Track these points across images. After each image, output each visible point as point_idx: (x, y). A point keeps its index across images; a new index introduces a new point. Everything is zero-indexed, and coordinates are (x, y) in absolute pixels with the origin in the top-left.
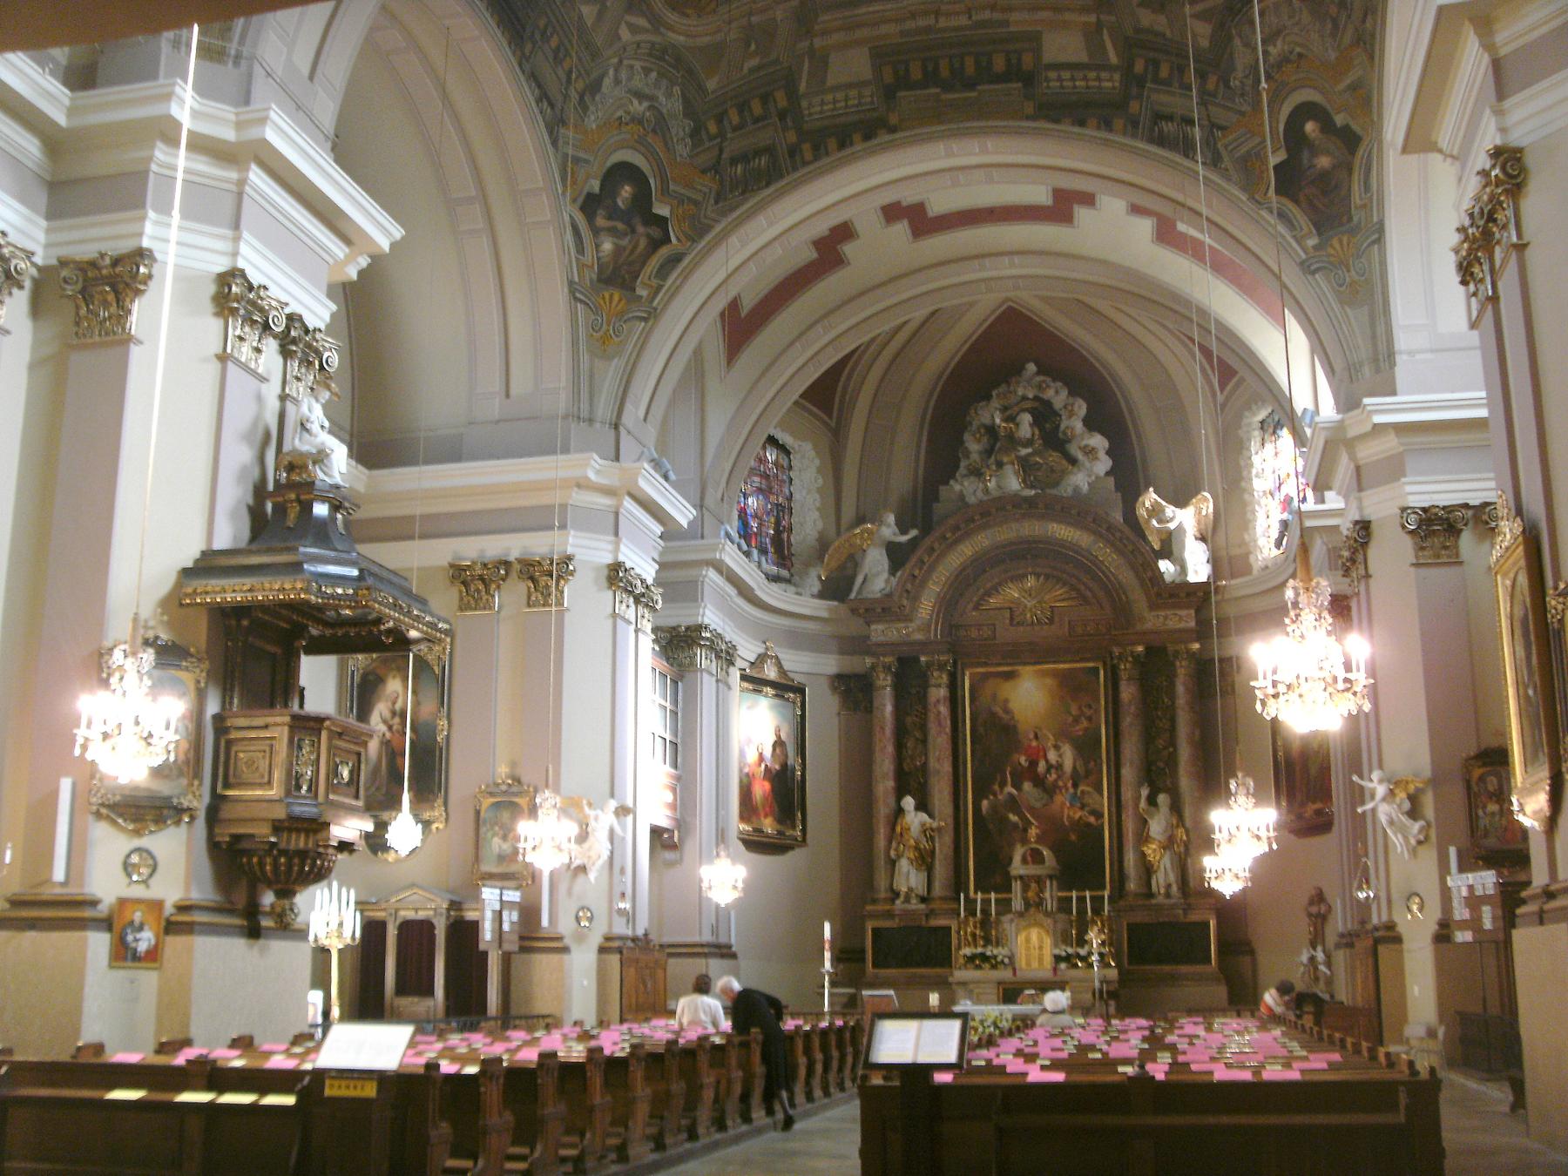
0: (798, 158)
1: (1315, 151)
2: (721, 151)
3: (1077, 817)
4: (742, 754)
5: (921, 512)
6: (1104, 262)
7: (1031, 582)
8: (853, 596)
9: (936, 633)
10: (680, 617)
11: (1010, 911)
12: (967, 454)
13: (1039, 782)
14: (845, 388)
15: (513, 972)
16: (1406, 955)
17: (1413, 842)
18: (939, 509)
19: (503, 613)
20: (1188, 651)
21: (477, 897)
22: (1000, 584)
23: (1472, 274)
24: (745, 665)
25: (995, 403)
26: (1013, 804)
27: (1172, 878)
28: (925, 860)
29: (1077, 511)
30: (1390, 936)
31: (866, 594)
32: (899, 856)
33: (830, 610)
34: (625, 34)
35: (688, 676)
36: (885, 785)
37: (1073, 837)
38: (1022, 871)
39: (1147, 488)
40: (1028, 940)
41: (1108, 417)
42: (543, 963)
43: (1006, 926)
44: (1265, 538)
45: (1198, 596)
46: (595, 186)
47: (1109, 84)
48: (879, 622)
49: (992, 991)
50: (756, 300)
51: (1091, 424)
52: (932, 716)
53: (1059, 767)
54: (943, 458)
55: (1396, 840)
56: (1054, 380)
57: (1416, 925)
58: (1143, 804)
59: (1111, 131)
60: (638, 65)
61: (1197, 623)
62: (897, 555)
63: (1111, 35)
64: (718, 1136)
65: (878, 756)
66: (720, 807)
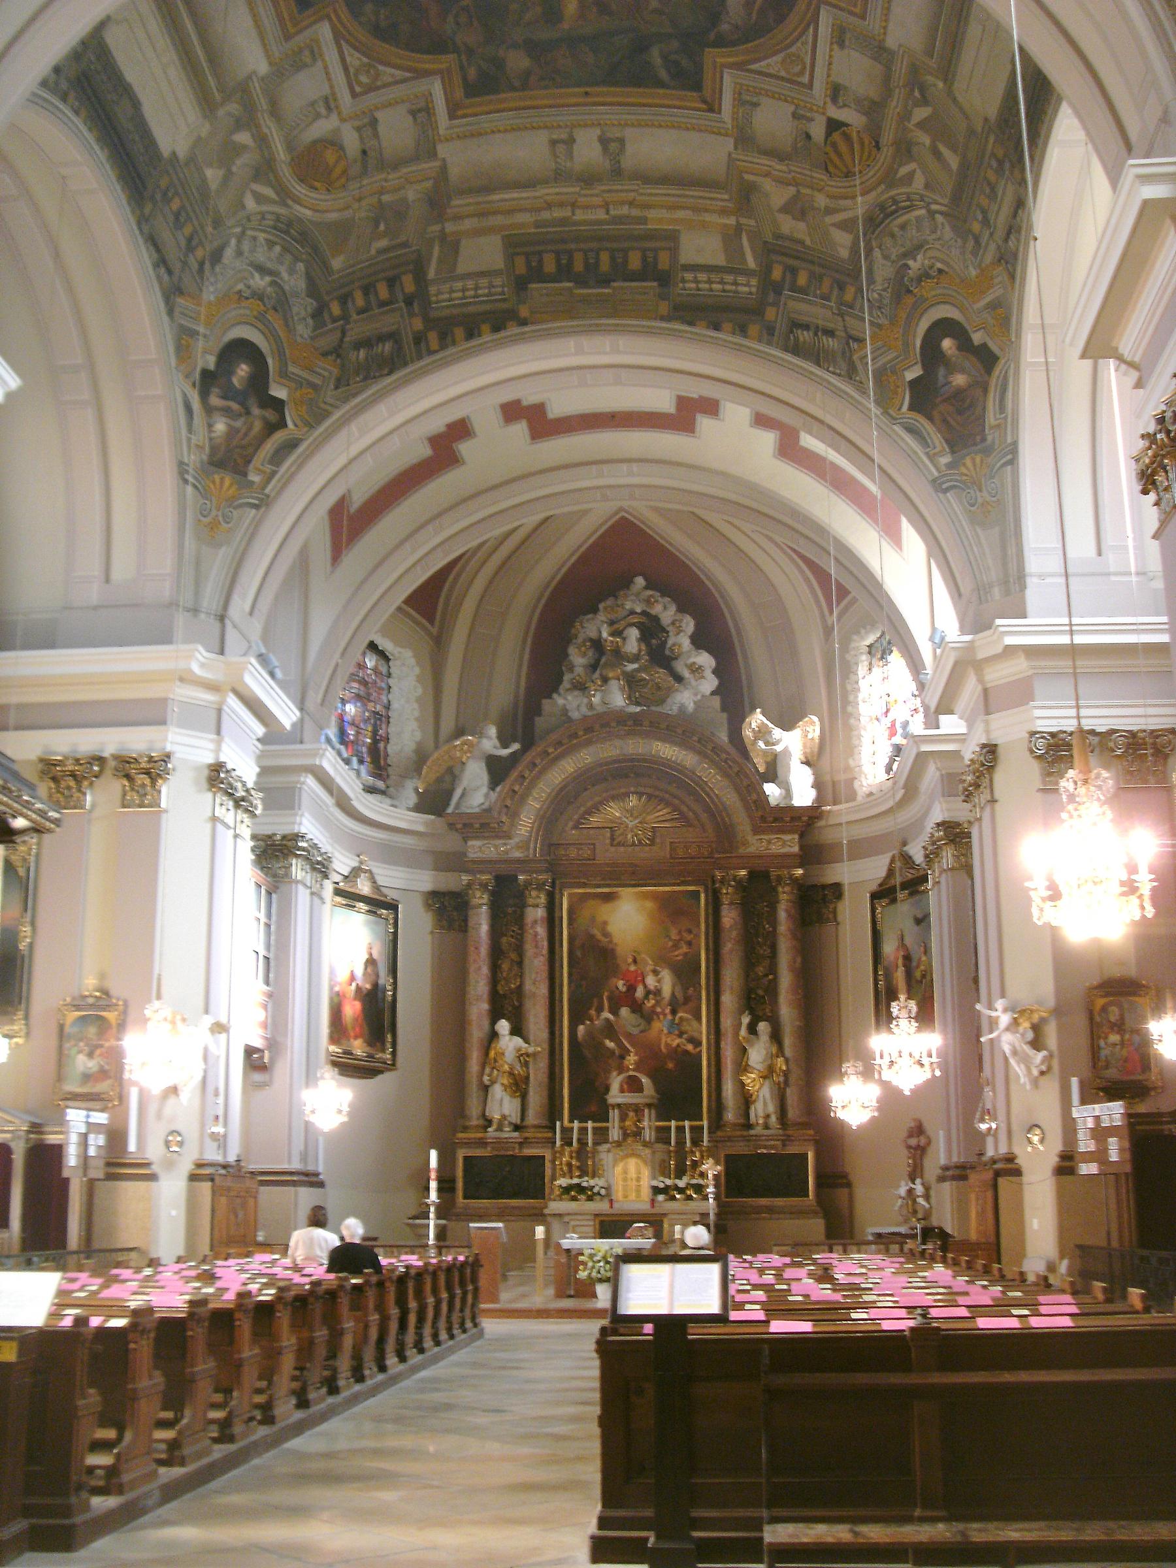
0: (423, 345)
1: (951, 368)
2: (344, 333)
3: (675, 1044)
4: (332, 972)
5: (523, 725)
6: (723, 474)
7: (633, 801)
8: (450, 810)
9: (536, 850)
10: (279, 827)
11: (606, 1141)
12: (571, 669)
13: (637, 1008)
14: (448, 599)
15: (97, 1201)
16: (1026, 1188)
17: (1035, 1072)
18: (540, 723)
19: (96, 814)
20: (791, 877)
21: (62, 1122)
22: (601, 803)
23: (1154, 483)
24: (338, 878)
25: (602, 616)
26: (610, 1030)
27: (771, 1108)
28: (519, 1086)
29: (681, 730)
30: (1009, 1168)
31: (464, 809)
32: (493, 1082)
33: (426, 824)
34: (250, 204)
35: (283, 888)
36: (479, 1008)
37: (670, 1065)
38: (620, 1100)
39: (753, 709)
40: (625, 1172)
41: (714, 635)
42: (130, 1190)
43: (603, 1156)
44: (872, 767)
45: (804, 822)
46: (211, 362)
47: (746, 289)
48: (476, 838)
49: (590, 1226)
50: (367, 496)
51: (699, 641)
52: (529, 937)
53: (658, 992)
54: (546, 669)
55: (1017, 1068)
56: (663, 595)
57: (1038, 1157)
58: (743, 1032)
59: (746, 337)
60: (262, 236)
61: (801, 848)
62: (498, 770)
63: (749, 240)
64: (358, 1387)
65: (472, 977)
66: (309, 1029)
